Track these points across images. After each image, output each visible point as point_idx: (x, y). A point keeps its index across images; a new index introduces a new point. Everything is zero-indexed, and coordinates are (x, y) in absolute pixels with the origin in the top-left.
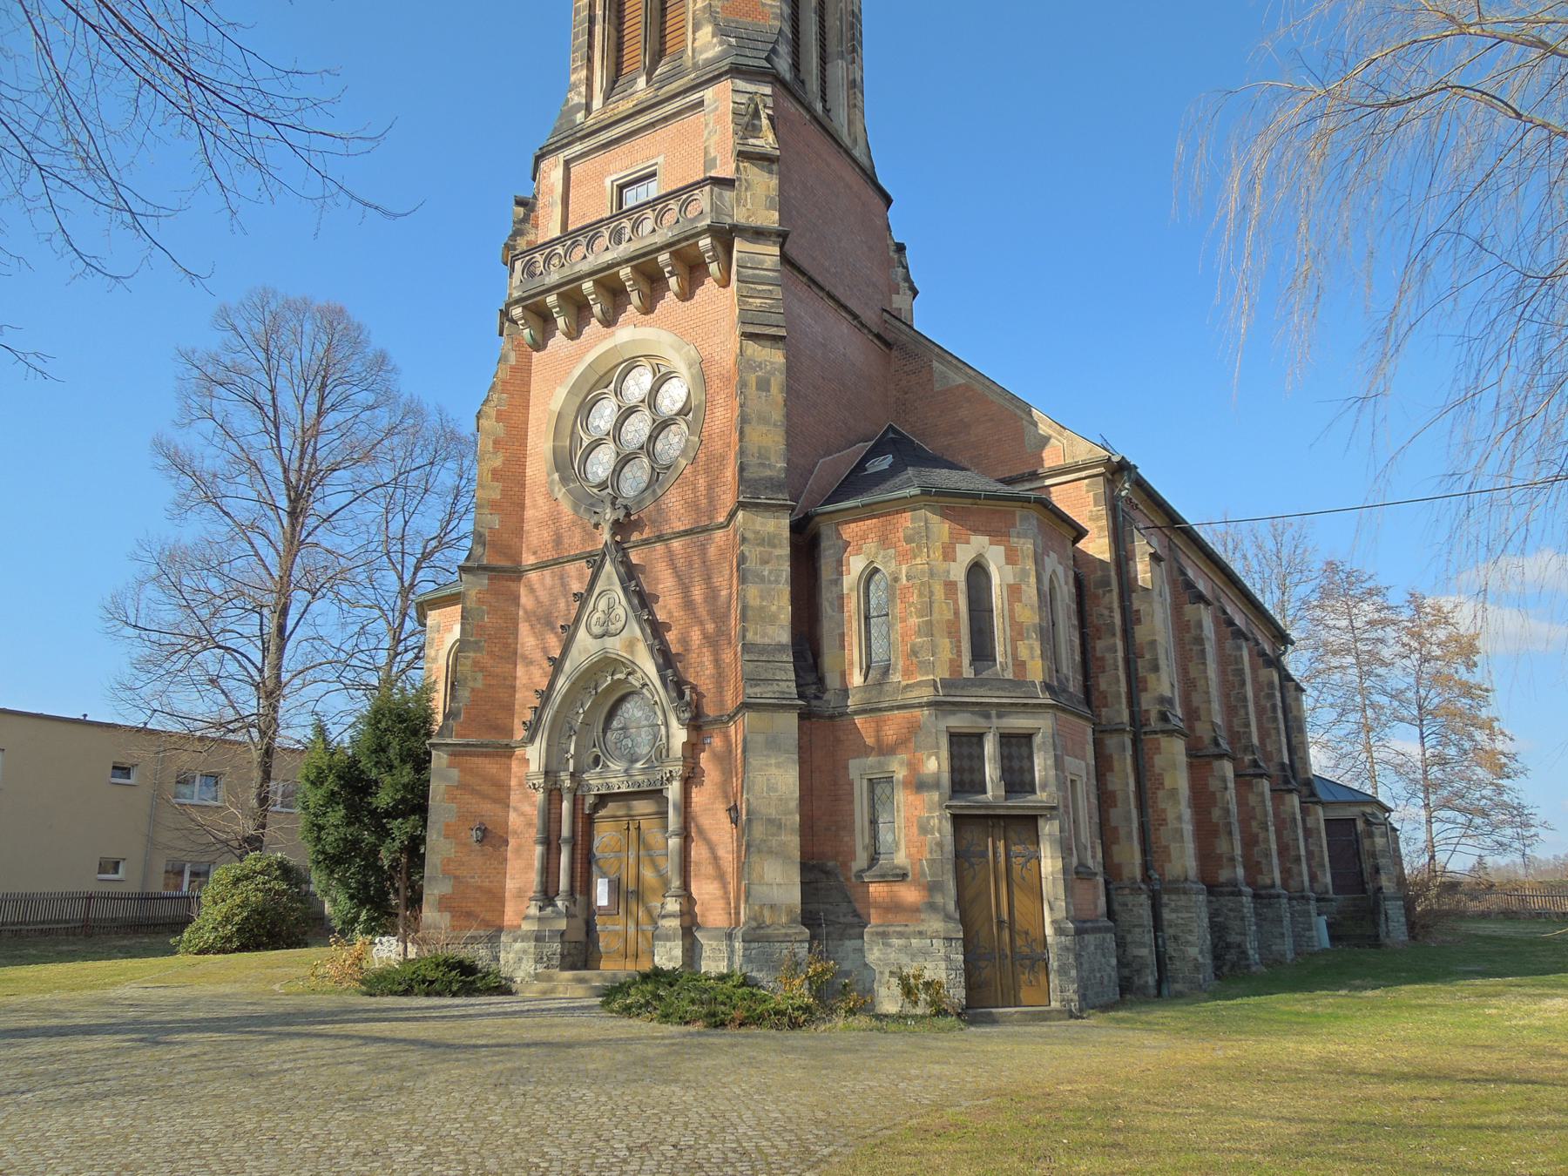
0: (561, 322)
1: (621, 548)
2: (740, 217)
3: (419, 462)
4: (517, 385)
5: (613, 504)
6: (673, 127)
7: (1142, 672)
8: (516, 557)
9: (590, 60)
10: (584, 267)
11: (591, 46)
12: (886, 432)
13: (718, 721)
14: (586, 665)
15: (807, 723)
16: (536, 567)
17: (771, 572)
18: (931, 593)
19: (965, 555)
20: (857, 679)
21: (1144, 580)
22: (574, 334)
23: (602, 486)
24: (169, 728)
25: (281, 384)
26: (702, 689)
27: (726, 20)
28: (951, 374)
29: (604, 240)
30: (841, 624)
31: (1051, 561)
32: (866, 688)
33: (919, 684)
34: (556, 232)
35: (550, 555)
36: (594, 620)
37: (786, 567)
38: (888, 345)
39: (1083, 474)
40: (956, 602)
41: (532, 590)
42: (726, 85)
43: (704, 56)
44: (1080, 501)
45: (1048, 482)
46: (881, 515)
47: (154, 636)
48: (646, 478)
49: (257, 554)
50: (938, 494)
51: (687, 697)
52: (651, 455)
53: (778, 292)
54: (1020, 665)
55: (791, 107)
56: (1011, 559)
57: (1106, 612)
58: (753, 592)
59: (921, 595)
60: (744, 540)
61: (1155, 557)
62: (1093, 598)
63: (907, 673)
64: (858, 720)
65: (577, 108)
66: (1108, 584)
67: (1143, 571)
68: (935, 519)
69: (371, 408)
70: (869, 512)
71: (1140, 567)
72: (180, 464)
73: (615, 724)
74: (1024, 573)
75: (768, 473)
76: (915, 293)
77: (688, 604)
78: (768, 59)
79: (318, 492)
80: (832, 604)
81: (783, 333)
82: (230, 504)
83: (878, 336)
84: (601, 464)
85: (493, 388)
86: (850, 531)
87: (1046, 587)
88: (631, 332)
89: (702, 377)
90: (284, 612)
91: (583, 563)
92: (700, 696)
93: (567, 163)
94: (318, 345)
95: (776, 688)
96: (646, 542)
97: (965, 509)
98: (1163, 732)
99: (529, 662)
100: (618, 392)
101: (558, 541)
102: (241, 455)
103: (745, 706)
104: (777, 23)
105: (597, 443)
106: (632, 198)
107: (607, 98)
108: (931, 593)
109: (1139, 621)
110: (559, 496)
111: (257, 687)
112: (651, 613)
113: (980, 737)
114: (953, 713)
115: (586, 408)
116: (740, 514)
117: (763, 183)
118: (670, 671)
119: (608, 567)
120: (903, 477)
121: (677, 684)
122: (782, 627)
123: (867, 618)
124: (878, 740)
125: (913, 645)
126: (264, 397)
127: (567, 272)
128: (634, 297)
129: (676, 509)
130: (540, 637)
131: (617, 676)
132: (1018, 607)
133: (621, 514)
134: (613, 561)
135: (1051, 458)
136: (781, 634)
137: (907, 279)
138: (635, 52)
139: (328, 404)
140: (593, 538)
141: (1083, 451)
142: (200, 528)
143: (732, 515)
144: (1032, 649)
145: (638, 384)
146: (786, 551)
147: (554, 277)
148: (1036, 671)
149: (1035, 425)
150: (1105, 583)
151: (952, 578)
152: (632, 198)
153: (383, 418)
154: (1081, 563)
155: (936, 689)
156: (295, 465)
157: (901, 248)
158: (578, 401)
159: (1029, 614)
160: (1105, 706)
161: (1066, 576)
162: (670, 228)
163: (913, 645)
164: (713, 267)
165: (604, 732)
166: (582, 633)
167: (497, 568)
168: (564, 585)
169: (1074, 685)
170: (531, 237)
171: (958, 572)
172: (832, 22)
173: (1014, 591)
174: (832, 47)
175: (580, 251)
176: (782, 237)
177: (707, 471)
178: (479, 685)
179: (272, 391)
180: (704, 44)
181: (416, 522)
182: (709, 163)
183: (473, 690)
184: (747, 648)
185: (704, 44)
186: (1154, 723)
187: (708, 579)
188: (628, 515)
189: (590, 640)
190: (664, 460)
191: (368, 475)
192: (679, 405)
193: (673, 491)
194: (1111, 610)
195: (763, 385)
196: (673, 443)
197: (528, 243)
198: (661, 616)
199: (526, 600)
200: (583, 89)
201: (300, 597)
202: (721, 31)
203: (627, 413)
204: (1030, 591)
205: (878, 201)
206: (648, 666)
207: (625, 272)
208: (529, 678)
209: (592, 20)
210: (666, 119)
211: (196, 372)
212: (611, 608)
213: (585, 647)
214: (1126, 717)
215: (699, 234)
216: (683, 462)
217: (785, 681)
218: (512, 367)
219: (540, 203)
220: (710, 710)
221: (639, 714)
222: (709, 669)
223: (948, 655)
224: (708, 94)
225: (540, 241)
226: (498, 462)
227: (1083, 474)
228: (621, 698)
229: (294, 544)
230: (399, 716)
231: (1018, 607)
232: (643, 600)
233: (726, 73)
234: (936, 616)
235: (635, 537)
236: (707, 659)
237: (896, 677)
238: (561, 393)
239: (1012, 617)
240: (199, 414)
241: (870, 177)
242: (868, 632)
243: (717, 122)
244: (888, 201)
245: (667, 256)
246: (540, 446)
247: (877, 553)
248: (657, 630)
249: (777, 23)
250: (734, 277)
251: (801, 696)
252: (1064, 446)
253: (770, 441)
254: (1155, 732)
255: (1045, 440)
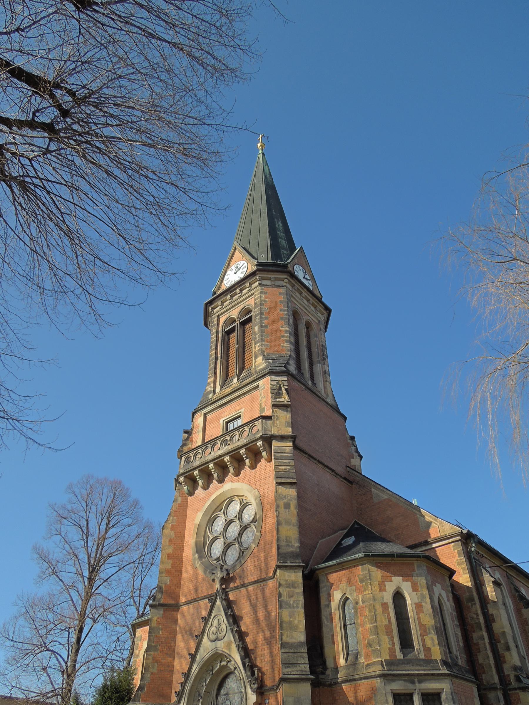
0: (200, 482)
1: (225, 592)
2: (275, 431)
3: (150, 550)
4: (181, 513)
5: (221, 569)
6: (248, 396)
7: (501, 651)
8: (176, 597)
9: (215, 373)
10: (210, 457)
11: (216, 368)
12: (354, 524)
13: (272, 689)
14: (207, 657)
15: (317, 689)
16: (188, 603)
17: (294, 602)
18: (375, 610)
19: (391, 588)
20: (342, 661)
21: (492, 596)
22: (206, 487)
23: (218, 559)
24: (19, 696)
25: (92, 516)
26: (264, 670)
27: (267, 353)
28: (381, 494)
29: (218, 446)
30: (332, 629)
31: (438, 589)
32: (347, 666)
33: (374, 663)
34: (200, 443)
35: (191, 597)
36: (211, 631)
37: (302, 599)
38: (351, 482)
39: (450, 540)
40: (389, 614)
41: (184, 616)
42: (268, 378)
43: (259, 368)
44: (451, 556)
45: (434, 545)
46: (348, 568)
47: (20, 645)
48: (237, 555)
49: (72, 600)
50: (372, 556)
51: (256, 675)
52: (240, 543)
53: (292, 463)
54: (427, 650)
55: (296, 384)
56: (415, 588)
57: (475, 616)
58: (285, 613)
59: (370, 611)
60: (280, 585)
61: (496, 583)
62: (464, 610)
63: (367, 657)
64: (344, 686)
65: (210, 392)
66: (473, 600)
67: (490, 591)
68: (373, 569)
69: (130, 525)
70: (341, 567)
71: (488, 589)
72: (44, 557)
73: (223, 692)
74: (423, 597)
75: (291, 549)
76: (361, 457)
77: (257, 621)
78: (285, 367)
79: (102, 569)
80: (327, 618)
81: (295, 481)
82: (62, 575)
83: (345, 479)
84: (217, 548)
85: (170, 515)
86: (333, 577)
87: (437, 604)
88: (231, 485)
89: (261, 504)
90: (81, 631)
91: (207, 600)
92: (263, 674)
93: (205, 415)
94: (109, 498)
95: (299, 668)
96: (237, 588)
97: (386, 562)
98: (520, 688)
99: (181, 657)
100: (225, 513)
101: (196, 589)
102: (71, 551)
103: (283, 680)
104: (289, 353)
105: (215, 539)
106: (231, 426)
107: (222, 387)
108: (375, 609)
109: (494, 621)
110: (198, 566)
111: (63, 673)
112: (238, 626)
113: (410, 696)
114: (394, 681)
115: (211, 521)
116: (278, 571)
117: (284, 416)
118: (247, 660)
119: (218, 602)
120: (358, 547)
121: (251, 667)
122: (301, 632)
123: (345, 626)
124: (356, 699)
125: (369, 640)
126: (84, 523)
127: (203, 460)
128: (231, 469)
129: (250, 571)
130: (186, 642)
131: (223, 663)
132: (422, 615)
133: (225, 574)
134: (220, 599)
135: (434, 533)
136: (299, 635)
137: (357, 451)
138: (233, 369)
139: (111, 524)
140: (213, 587)
141: (448, 528)
142: (50, 587)
143: (275, 572)
144: (433, 640)
145: (235, 507)
146: (301, 590)
147: (197, 463)
148: (437, 654)
149: (424, 517)
150: (472, 599)
151: (385, 601)
152: (231, 426)
153: (135, 530)
154: (455, 589)
155: (383, 666)
156: (93, 555)
157: (353, 438)
158: (208, 518)
159: (429, 620)
160: (484, 673)
161: (448, 597)
162: (245, 438)
163: (369, 640)
164: (264, 454)
165: (217, 697)
166: (205, 640)
167: (166, 603)
168: (199, 612)
169: (462, 661)
170: (190, 446)
171: (388, 598)
172: (314, 350)
173: (419, 607)
174: (315, 359)
175: (209, 450)
176: (293, 438)
177: (265, 550)
178: (155, 670)
179: (87, 520)
180: (259, 363)
181: (147, 580)
182: (262, 410)
183: (152, 673)
184: (284, 645)
185: (259, 363)
186: (514, 684)
187: (266, 607)
188: (228, 574)
189: (209, 643)
190: (245, 546)
191: (127, 557)
192: (251, 519)
193: (249, 561)
194: (477, 615)
195: (287, 506)
196: (248, 537)
197: (188, 448)
198: (243, 629)
199: (180, 621)
200: (212, 385)
201: (88, 622)
202: (266, 358)
203: (229, 523)
204: (427, 606)
205: (341, 419)
206: (237, 657)
207: (227, 459)
208: (180, 665)
209: (216, 359)
210: (244, 394)
211: (55, 513)
212: (219, 624)
213: (207, 647)
214: (496, 680)
215: (257, 440)
216: (253, 546)
217: (304, 666)
218: (179, 504)
219: (194, 432)
220: (268, 683)
221: (234, 685)
222: (267, 658)
223: (388, 646)
224: (261, 382)
225: (193, 447)
226: (170, 550)
227: (450, 540)
228: (226, 675)
229: (89, 595)
230: (116, 689)
231: (422, 615)
232: (235, 620)
233: (267, 374)
234: (379, 623)
235: (232, 585)
236: (266, 652)
237: (362, 660)
238: (200, 515)
239: (420, 622)
240: (55, 532)
241: (336, 409)
242: (346, 633)
243: (264, 393)
244: (345, 418)
245: (244, 450)
246: (190, 541)
247: (346, 589)
248: (241, 636)
249: (289, 353)
250: (273, 458)
251: (312, 672)
252: (439, 527)
253: (291, 533)
254: (515, 689)
255: (429, 524)
